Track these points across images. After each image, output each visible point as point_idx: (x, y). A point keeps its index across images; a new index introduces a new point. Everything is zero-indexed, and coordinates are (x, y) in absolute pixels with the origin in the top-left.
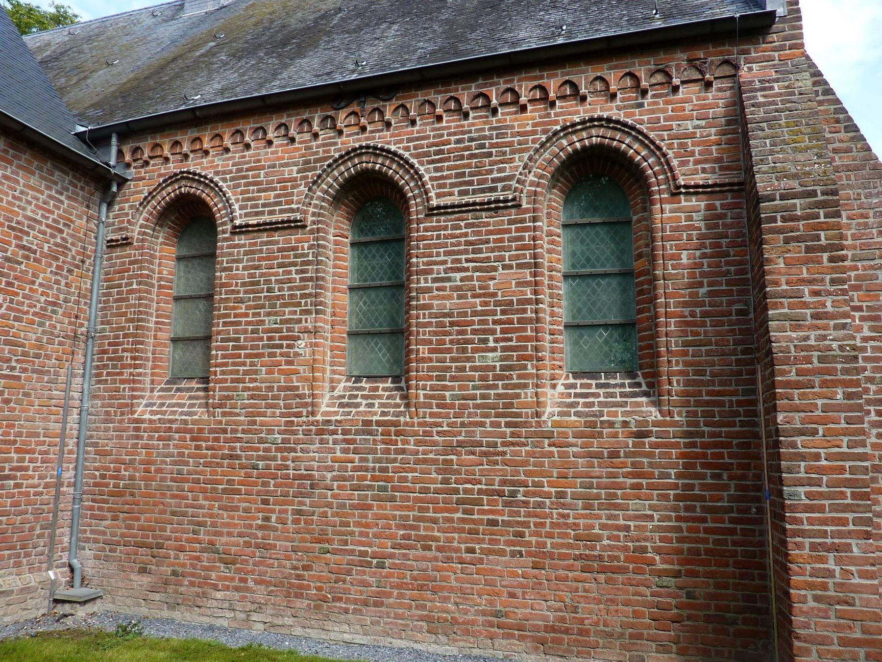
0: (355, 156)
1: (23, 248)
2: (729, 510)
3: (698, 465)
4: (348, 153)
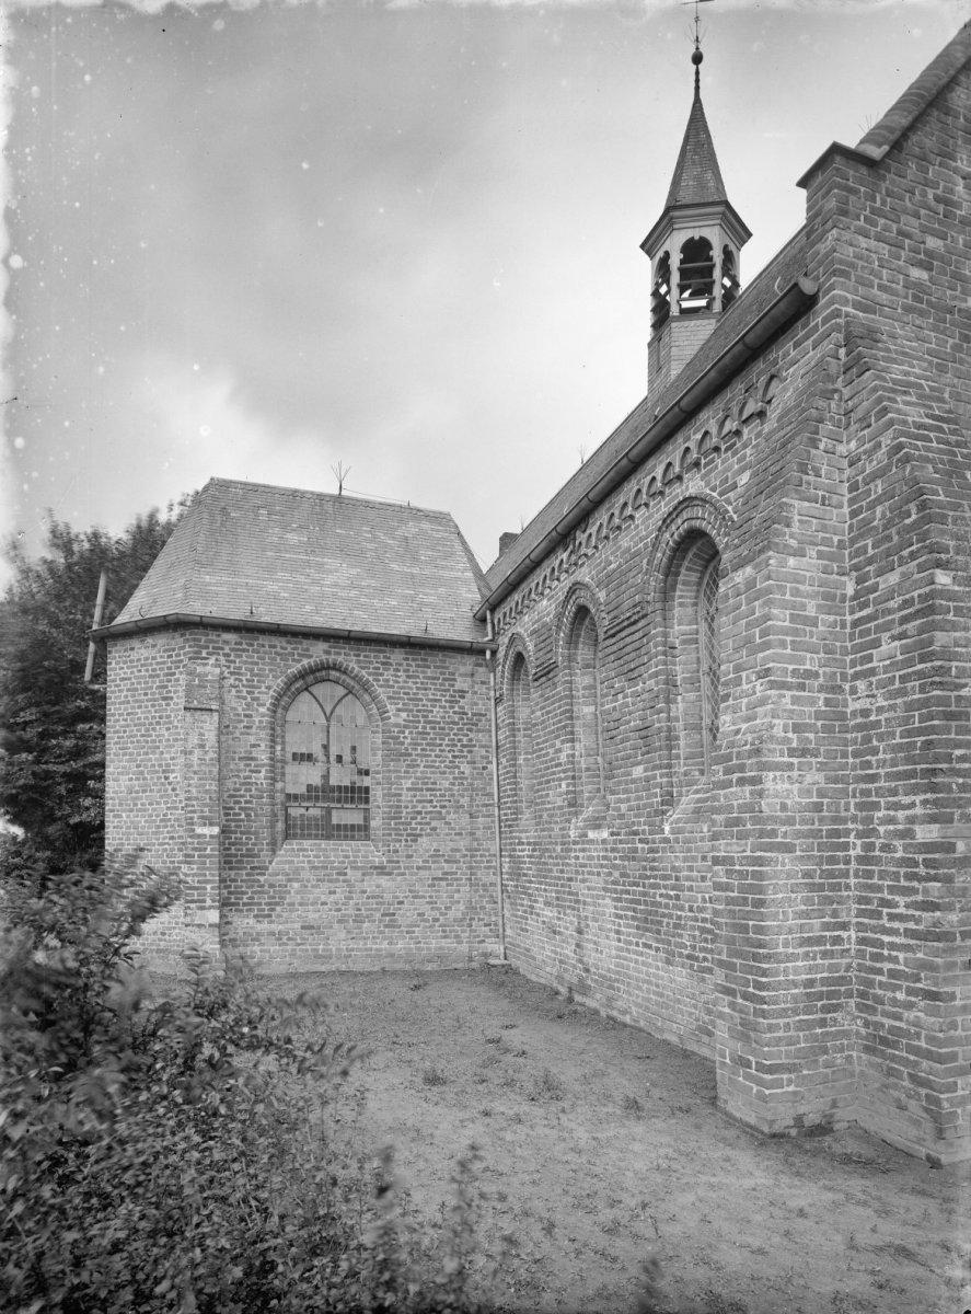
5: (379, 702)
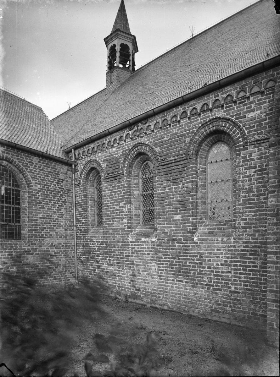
0: (136, 147)
1: (49, 190)
2: (259, 271)
3: (239, 258)
4: (134, 147)
5: (28, 179)
